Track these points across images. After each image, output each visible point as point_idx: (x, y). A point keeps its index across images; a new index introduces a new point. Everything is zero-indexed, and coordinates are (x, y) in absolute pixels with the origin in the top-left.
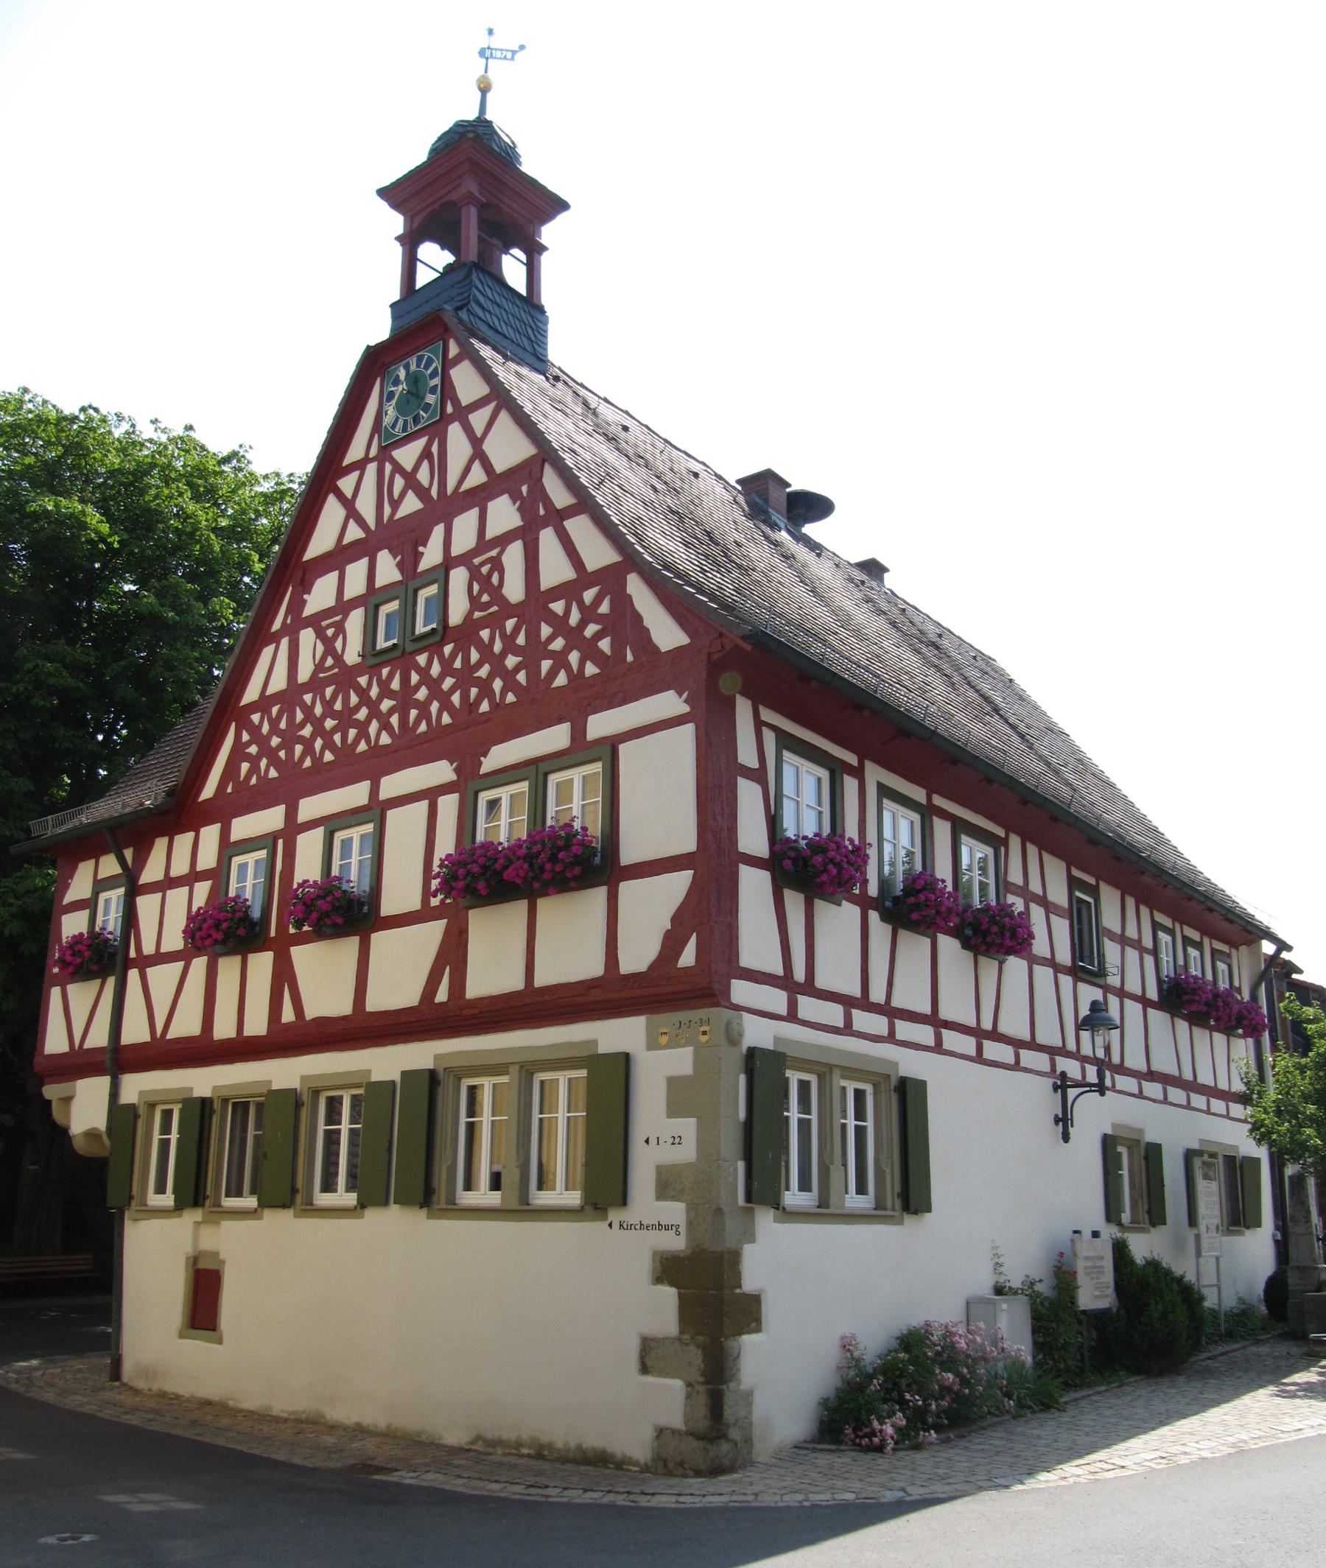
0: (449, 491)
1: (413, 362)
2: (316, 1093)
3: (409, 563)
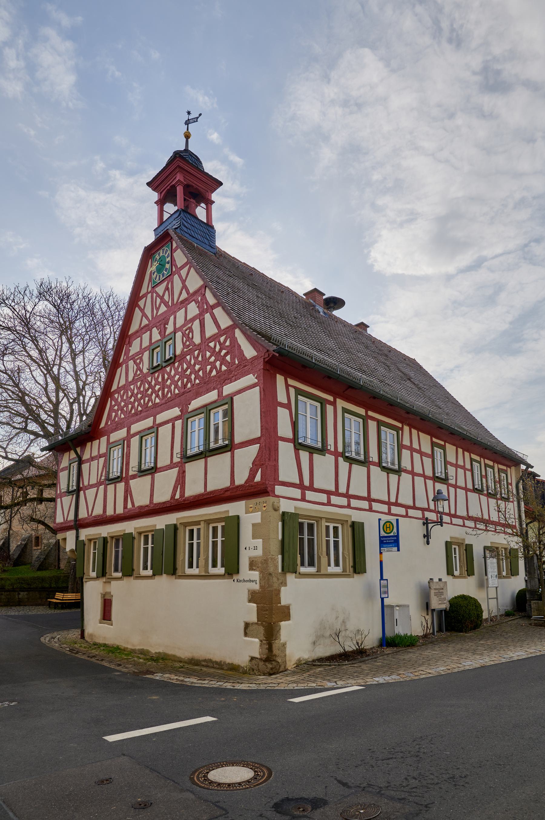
2: (140, 533)
3: (162, 333)
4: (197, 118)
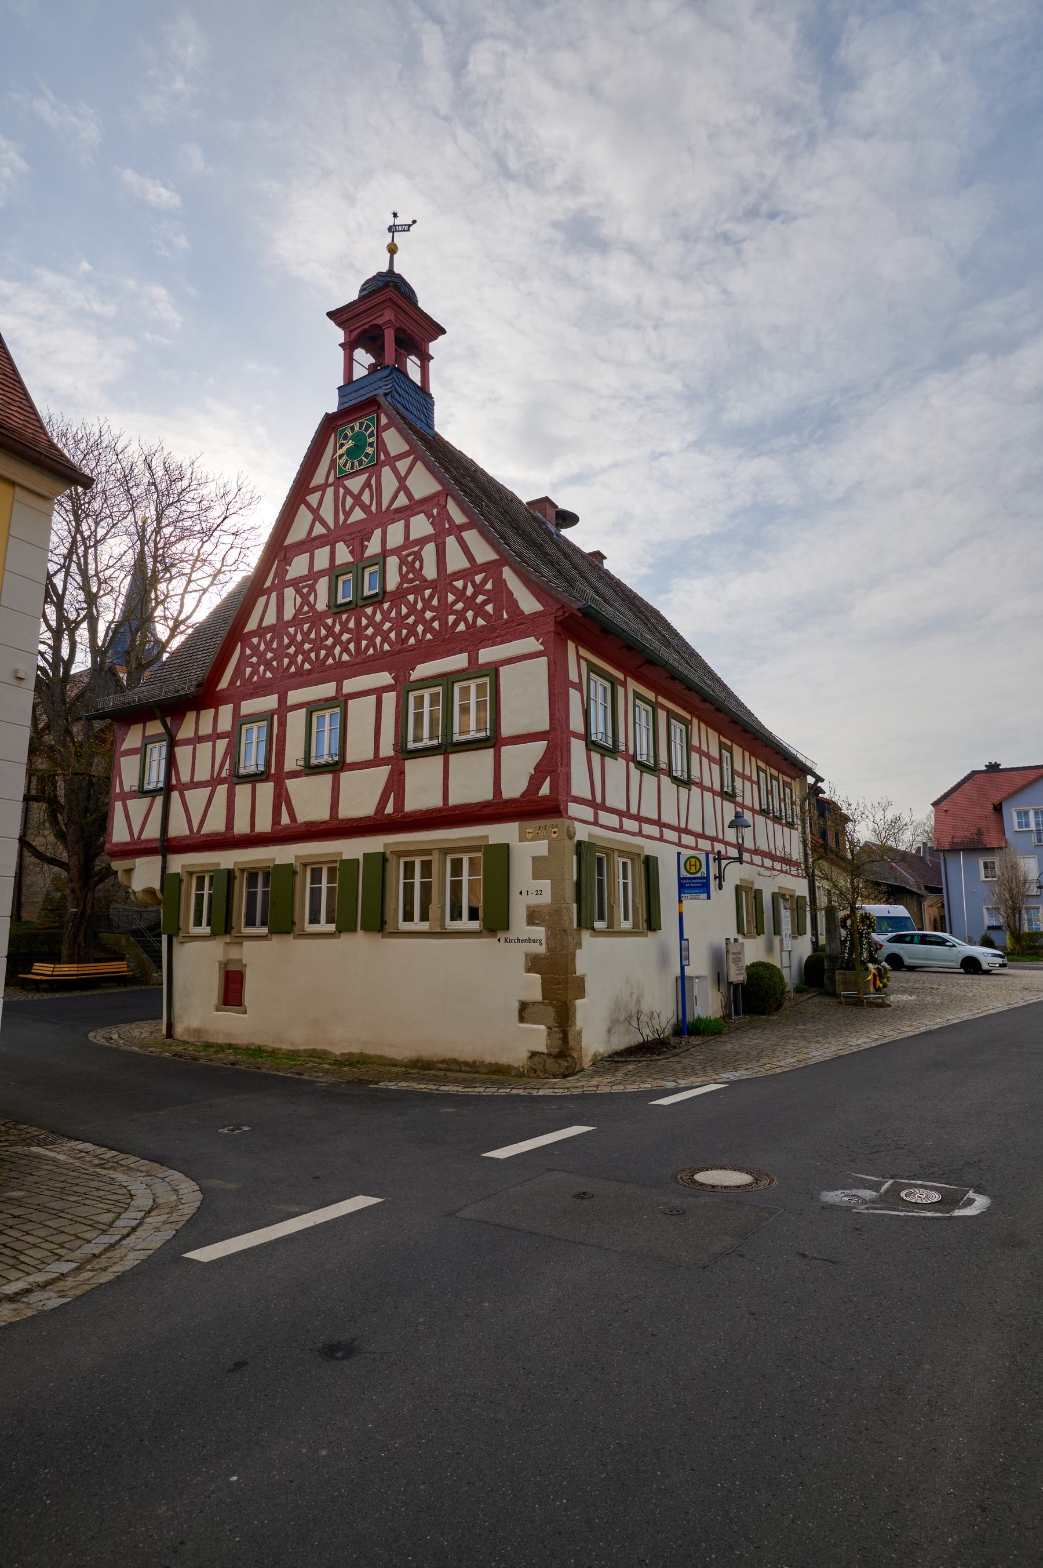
0: (384, 509)
1: (357, 425)
3: (358, 551)
4: (409, 226)
